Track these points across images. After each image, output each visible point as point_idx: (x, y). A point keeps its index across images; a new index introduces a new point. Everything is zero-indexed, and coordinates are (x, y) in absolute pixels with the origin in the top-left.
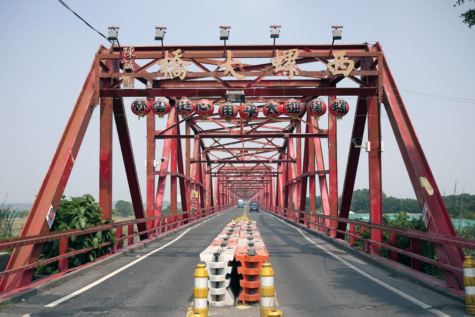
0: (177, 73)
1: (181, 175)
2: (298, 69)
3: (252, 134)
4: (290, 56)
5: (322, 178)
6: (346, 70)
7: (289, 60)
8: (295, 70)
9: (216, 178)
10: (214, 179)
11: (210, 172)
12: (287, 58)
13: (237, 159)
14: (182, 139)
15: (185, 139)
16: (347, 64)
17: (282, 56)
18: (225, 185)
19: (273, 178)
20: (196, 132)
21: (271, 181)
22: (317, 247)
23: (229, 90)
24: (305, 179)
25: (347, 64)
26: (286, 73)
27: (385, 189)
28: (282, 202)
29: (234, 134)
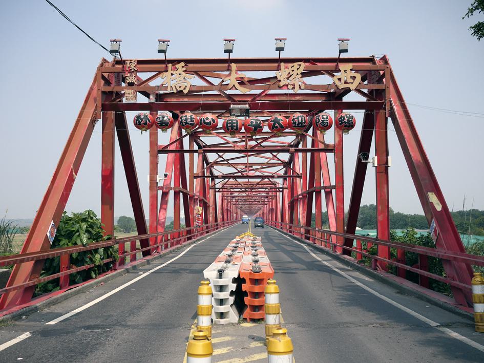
0: (180, 87)
1: (185, 191)
2: (303, 83)
3: (257, 148)
4: (296, 70)
5: (328, 194)
6: (352, 83)
7: (295, 73)
8: (300, 83)
9: (220, 193)
10: (218, 195)
11: (214, 188)
12: (293, 71)
14: (185, 154)
16: (354, 78)
19: (278, 193)
20: (200, 147)
22: (322, 263)
23: (233, 104)
24: (310, 195)
25: (354, 78)
26: (292, 87)
27: (392, 205)
29: (239, 149)
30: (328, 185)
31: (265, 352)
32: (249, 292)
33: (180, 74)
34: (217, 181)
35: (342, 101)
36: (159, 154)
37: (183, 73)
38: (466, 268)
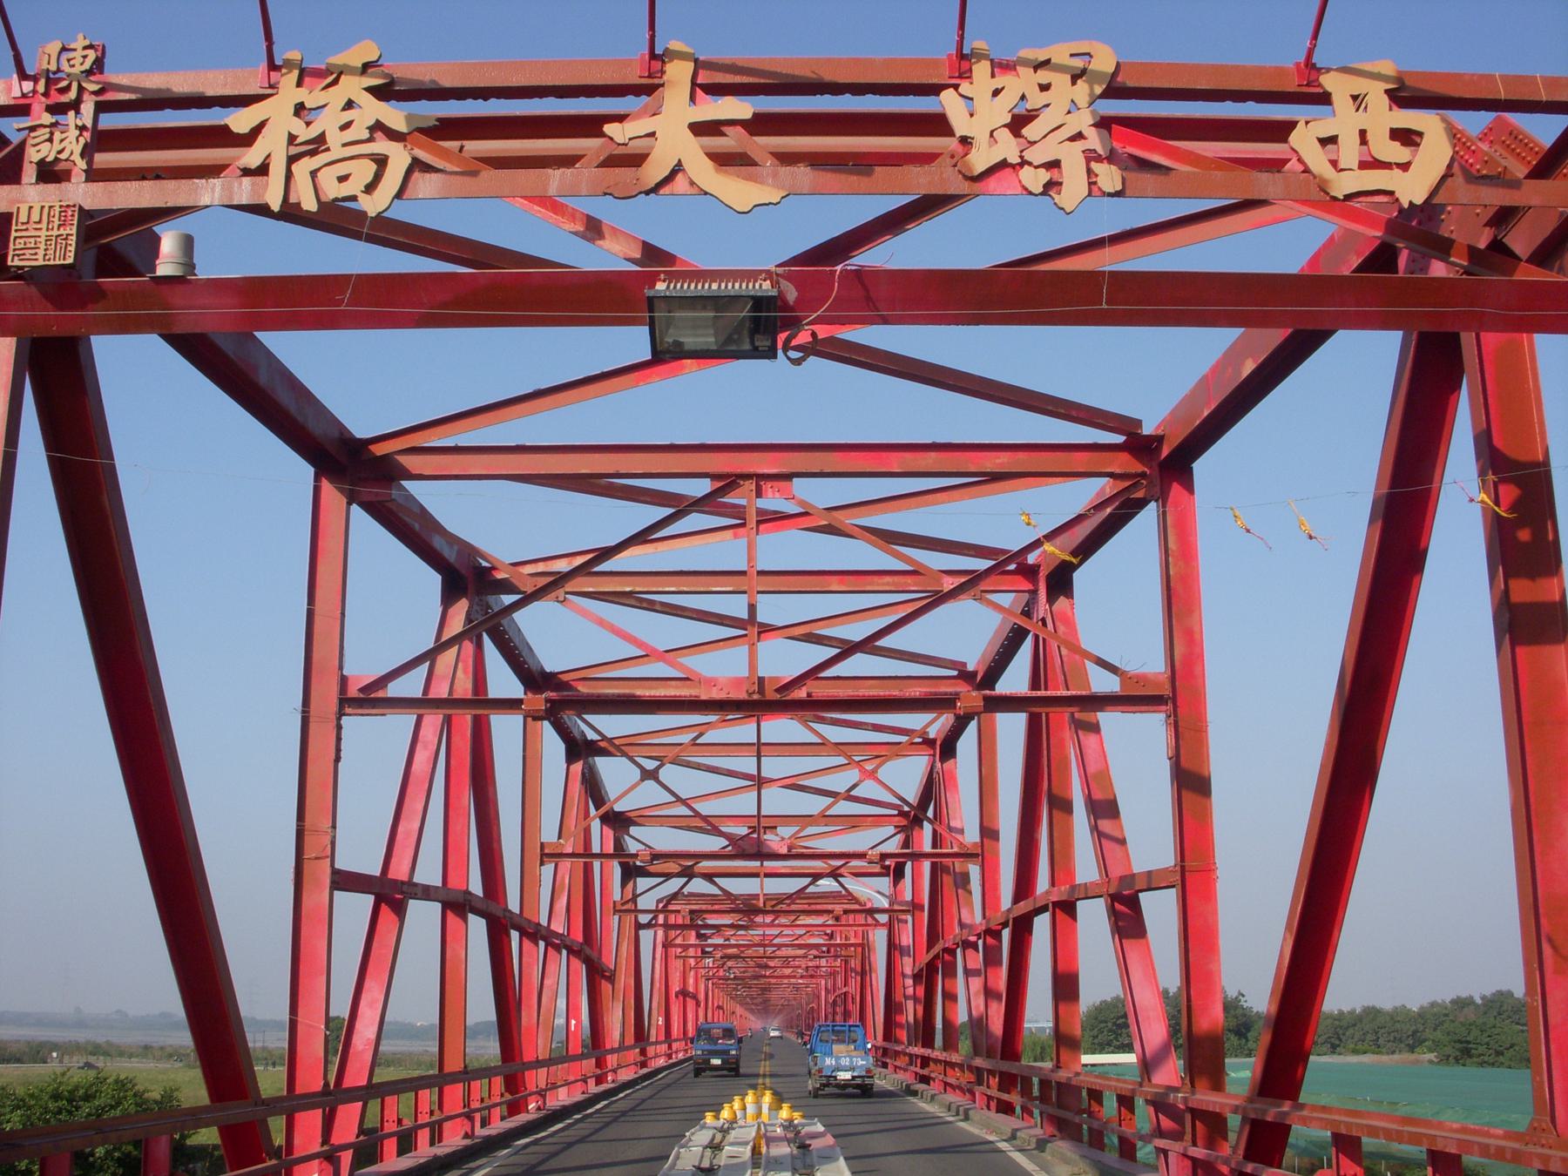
0: (343, 179)
1: (494, 908)
3: (801, 694)
6: (1405, 167)
11: (629, 906)
12: (1045, 88)
13: (752, 920)
15: (594, 851)
18: (692, 962)
20: (534, 678)
24: (1022, 928)
25: (1407, 137)
26: (1044, 176)
27: (303, 1114)
29: (722, 696)
31: (788, 1171)
33: (349, 105)
34: (643, 883)
37: (367, 100)
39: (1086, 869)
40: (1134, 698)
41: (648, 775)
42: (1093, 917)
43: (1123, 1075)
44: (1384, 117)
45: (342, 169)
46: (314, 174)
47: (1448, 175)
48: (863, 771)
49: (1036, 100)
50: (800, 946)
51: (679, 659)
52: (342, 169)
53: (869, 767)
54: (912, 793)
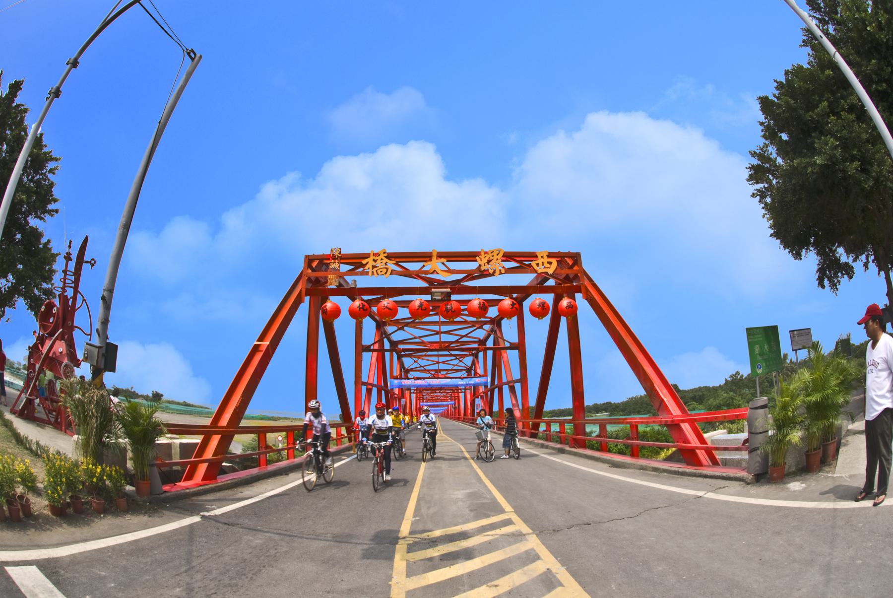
0: (381, 272)
2: (503, 267)
4: (495, 255)
5: (512, 390)
6: (549, 268)
7: (495, 258)
8: (500, 268)
9: (415, 395)
10: (414, 396)
12: (493, 256)
14: (386, 353)
16: (550, 263)
17: (487, 255)
19: (460, 394)
21: (459, 397)
22: (527, 451)
23: (434, 288)
25: (550, 263)
28: (469, 411)
30: (511, 380)
32: (258, 341)
33: (382, 259)
35: (486, 346)
36: (363, 353)
37: (384, 258)
38: (744, 458)
39: (504, 380)
40: (513, 347)
41: (415, 362)
42: (506, 389)
43: (887, 347)
44: (546, 260)
45: (381, 270)
46: (376, 271)
47: (556, 268)
48: (460, 360)
49: (491, 258)
50: (445, 397)
51: (354, 267)
52: (381, 270)
53: (461, 359)
54: (469, 365)
